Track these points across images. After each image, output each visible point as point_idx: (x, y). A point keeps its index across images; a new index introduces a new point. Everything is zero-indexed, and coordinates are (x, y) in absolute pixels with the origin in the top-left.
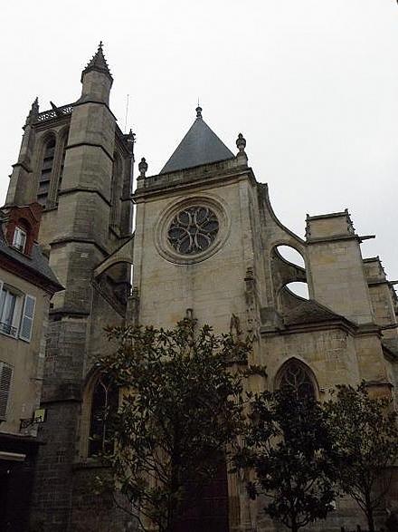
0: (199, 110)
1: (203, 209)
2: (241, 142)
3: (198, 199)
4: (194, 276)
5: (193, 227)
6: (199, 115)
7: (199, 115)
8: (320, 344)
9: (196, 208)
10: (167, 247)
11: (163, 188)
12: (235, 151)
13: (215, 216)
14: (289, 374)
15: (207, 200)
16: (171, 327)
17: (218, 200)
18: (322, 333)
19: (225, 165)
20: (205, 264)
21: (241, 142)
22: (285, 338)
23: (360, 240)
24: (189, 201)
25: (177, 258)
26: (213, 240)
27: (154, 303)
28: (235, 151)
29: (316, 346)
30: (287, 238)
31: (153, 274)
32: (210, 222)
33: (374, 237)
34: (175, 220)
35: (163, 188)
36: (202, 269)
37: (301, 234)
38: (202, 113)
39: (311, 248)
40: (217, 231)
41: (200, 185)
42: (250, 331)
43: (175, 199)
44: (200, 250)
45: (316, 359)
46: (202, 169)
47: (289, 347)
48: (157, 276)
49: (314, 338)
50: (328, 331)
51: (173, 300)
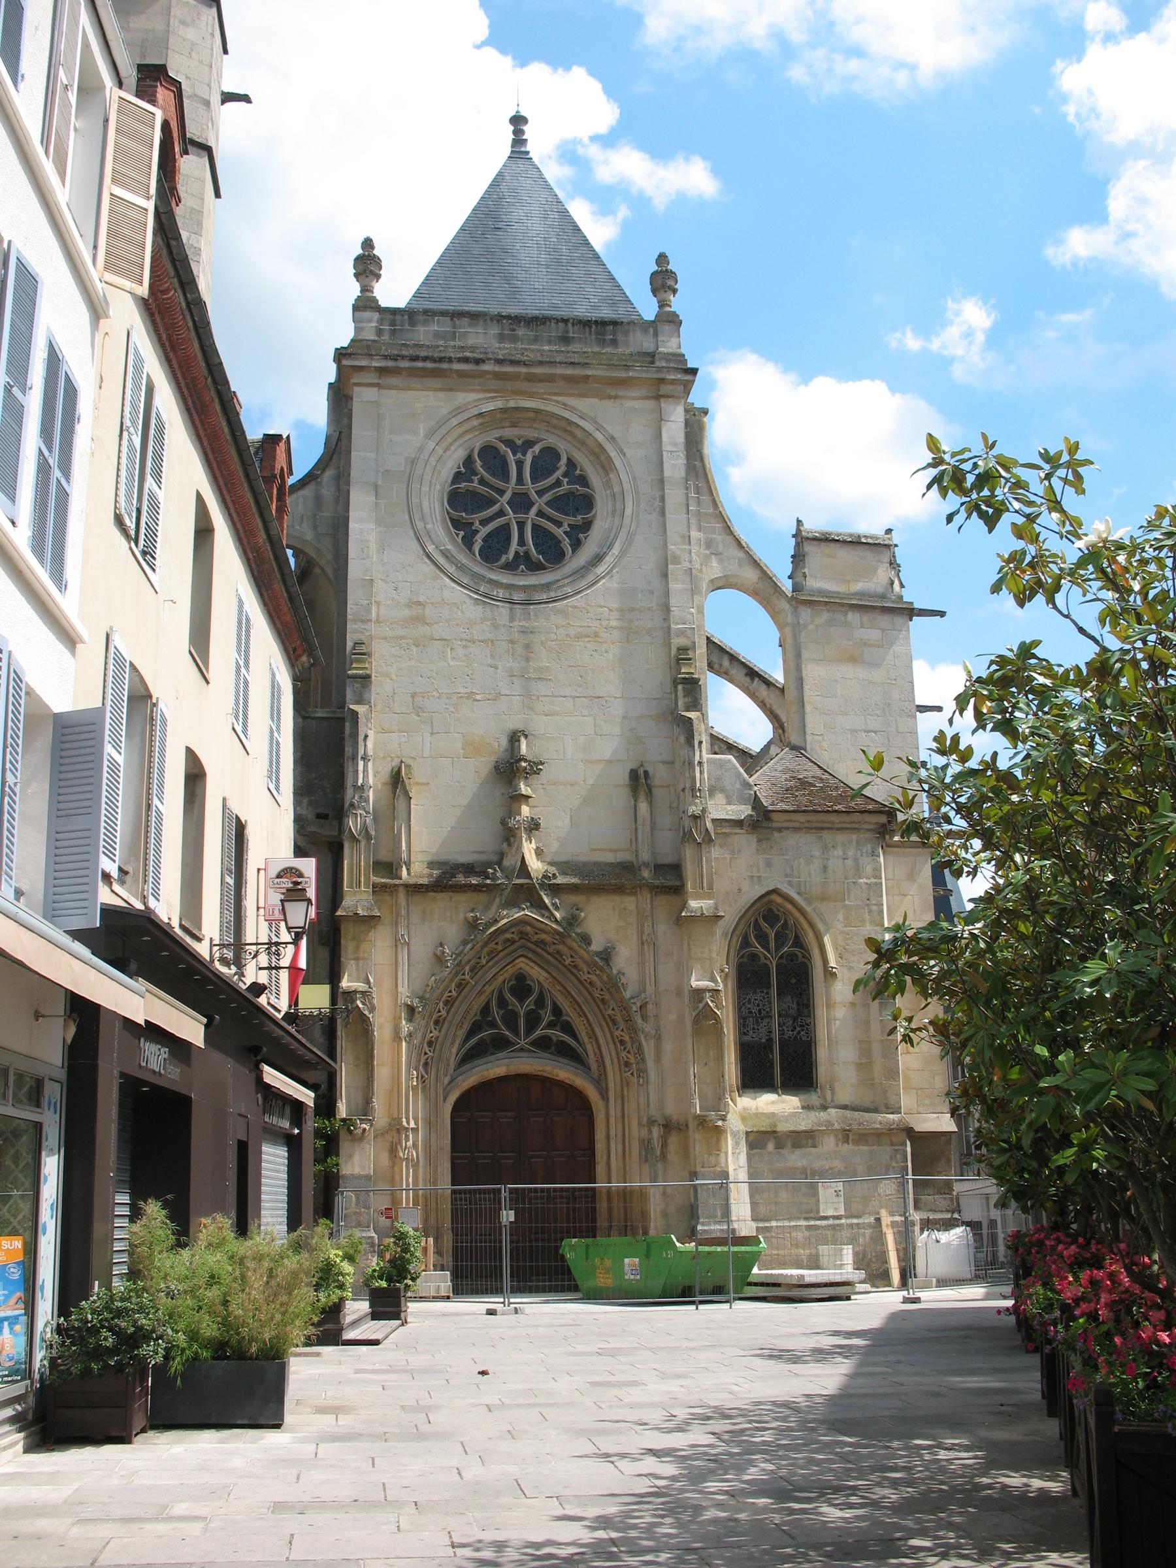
0: (518, 121)
1: (551, 453)
2: (663, 281)
6: (519, 140)
7: (519, 140)
8: (835, 864)
9: (529, 444)
11: (441, 360)
12: (648, 308)
13: (583, 481)
14: (502, 1002)
15: (567, 428)
16: (930, 917)
17: (599, 437)
18: (841, 837)
19: (620, 338)
20: (563, 613)
21: (663, 281)
22: (759, 841)
23: (911, 612)
24: (510, 416)
25: (475, 576)
26: (576, 545)
27: (413, 695)
28: (648, 308)
29: (825, 869)
30: (751, 575)
31: (406, 612)
32: (570, 495)
33: (942, 614)
34: (468, 462)
35: (441, 360)
36: (551, 622)
37: (781, 569)
38: (529, 131)
39: (805, 613)
40: (587, 526)
41: (550, 379)
43: (477, 400)
44: (535, 567)
45: (824, 898)
46: (554, 331)
47: (768, 864)
48: (420, 620)
49: (825, 849)
50: (854, 837)
51: (470, 695)
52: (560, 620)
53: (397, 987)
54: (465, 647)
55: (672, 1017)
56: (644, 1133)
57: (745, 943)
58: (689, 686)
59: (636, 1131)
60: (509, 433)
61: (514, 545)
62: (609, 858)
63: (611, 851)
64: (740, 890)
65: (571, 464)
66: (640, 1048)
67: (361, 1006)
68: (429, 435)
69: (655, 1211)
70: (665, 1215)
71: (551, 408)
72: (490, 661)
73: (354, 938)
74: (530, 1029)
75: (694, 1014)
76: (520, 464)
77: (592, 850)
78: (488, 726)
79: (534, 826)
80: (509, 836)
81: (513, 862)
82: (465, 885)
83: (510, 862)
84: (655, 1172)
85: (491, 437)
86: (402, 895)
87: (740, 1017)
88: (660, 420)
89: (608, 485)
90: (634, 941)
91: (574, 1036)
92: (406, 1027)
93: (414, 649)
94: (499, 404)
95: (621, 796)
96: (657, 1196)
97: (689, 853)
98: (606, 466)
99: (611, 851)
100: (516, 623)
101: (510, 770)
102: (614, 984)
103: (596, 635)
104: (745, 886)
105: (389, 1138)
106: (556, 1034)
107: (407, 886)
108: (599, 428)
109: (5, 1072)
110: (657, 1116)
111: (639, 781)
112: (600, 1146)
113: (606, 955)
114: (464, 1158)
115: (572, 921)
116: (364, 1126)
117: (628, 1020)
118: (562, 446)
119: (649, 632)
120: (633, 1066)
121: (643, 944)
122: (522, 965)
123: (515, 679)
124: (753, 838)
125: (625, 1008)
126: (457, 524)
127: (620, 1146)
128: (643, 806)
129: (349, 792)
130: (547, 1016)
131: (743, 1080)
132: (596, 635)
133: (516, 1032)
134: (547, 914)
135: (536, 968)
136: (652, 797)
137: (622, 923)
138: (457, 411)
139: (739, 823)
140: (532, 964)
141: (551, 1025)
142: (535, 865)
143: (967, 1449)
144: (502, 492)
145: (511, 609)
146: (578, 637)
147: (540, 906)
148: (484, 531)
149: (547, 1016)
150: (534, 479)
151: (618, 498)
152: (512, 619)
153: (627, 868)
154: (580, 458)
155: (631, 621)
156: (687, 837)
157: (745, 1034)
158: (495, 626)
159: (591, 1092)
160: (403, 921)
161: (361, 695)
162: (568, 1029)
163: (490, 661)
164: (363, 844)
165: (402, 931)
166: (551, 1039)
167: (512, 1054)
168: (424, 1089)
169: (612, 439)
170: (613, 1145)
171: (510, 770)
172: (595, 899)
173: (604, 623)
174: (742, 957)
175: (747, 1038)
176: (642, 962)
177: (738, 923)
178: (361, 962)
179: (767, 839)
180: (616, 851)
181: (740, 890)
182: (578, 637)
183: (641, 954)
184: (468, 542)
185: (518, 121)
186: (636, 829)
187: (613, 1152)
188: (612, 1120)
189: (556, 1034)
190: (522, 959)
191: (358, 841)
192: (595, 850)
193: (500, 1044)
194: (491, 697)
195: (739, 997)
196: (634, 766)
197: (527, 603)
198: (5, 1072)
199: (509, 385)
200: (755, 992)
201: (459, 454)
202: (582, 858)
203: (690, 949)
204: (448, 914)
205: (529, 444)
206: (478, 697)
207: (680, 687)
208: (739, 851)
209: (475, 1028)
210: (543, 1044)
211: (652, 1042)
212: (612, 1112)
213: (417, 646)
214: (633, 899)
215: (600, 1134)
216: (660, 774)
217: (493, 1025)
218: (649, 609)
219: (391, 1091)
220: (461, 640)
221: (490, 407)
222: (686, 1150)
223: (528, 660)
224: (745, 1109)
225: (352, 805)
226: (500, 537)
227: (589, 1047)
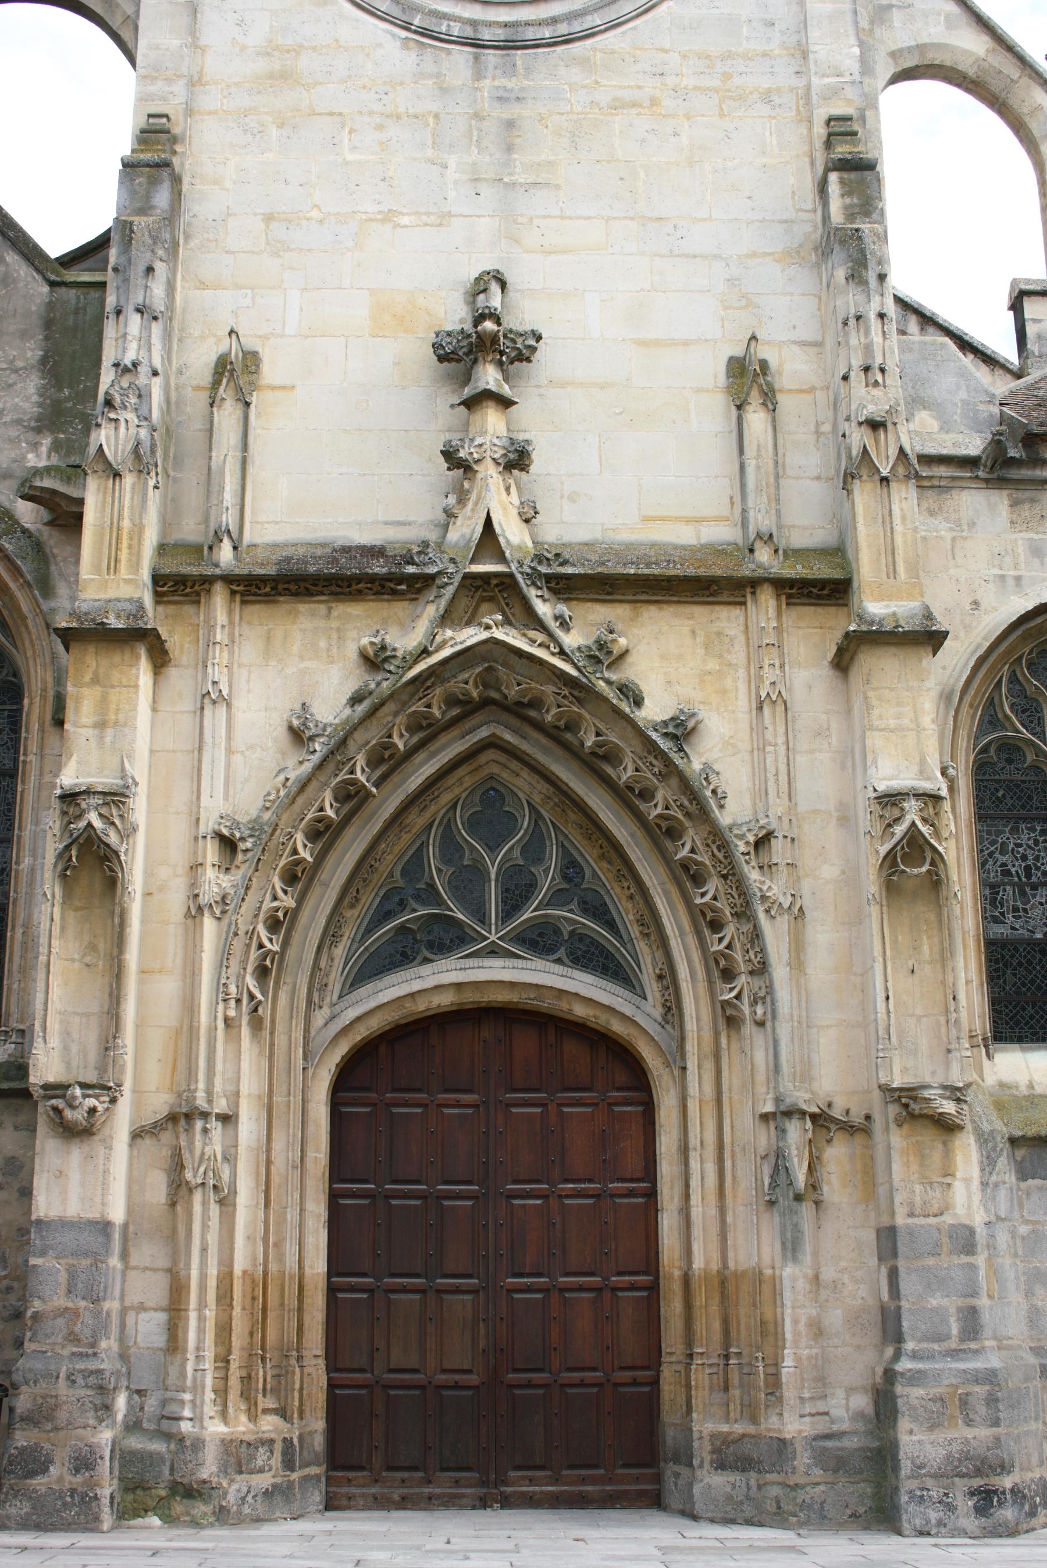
4: (513, 111)
14: (450, 847)
20: (584, 62)
22: (1015, 504)
42: (875, 425)
48: (284, 77)
51: (388, 217)
52: (576, 75)
53: (198, 798)
54: (380, 128)
55: (829, 871)
56: (763, 1139)
57: (991, 719)
58: (853, 175)
59: (749, 1135)
63: (689, 521)
64: (976, 603)
66: (756, 936)
67: (98, 824)
69: (795, 1322)
70: (818, 1330)
72: (430, 153)
73: (95, 681)
74: (511, 907)
75: (884, 850)
77: (646, 519)
81: (467, 531)
82: (359, 579)
84: (797, 1229)
86: (219, 597)
87: (985, 883)
90: (742, 703)
91: (611, 925)
92: (215, 882)
93: (274, 131)
95: (711, 411)
96: (801, 1284)
99: (689, 521)
100: (487, 83)
102: (697, 801)
103: (654, 102)
104: (988, 596)
105: (166, 1137)
106: (570, 916)
107: (229, 579)
110: (801, 1098)
112: (667, 1169)
113: (682, 730)
114: (528, 1289)
116: (92, 1102)
117: (732, 875)
119: (766, 97)
120: (738, 972)
121: (760, 708)
122: (495, 769)
123: (485, 189)
124: (1000, 500)
125: (718, 839)
127: (711, 1168)
129: (107, 377)
130: (548, 880)
131: (995, 1022)
132: (654, 102)
133: (483, 920)
134: (541, 637)
135: (525, 773)
136: (775, 404)
137: (713, 665)
139: (969, 462)
140: (515, 765)
141: (557, 898)
145: (476, 58)
146: (618, 105)
149: (548, 880)
152: (478, 76)
155: (727, 76)
157: (995, 920)
158: (444, 90)
160: (220, 656)
161: (148, 197)
162: (600, 912)
163: (430, 153)
164: (129, 480)
165: (217, 673)
166: (557, 931)
167: (470, 962)
168: (257, 1024)
170: (694, 1164)
171: (481, 353)
172: (650, 613)
173: (671, 81)
174: (985, 750)
175: (1000, 931)
176: (760, 747)
177: (975, 669)
178: (109, 733)
179: (1033, 501)
180: (699, 520)
181: (976, 603)
182: (618, 105)
183: (758, 729)
186: (742, 467)
187: (695, 1182)
188: (693, 1106)
189: (570, 916)
190: (491, 754)
191: (117, 475)
192: (654, 519)
193: (445, 938)
194: (432, 219)
195: (980, 840)
196: (739, 351)
197: (510, 45)
200: (1015, 830)
202: (624, 536)
203: (869, 707)
204: (323, 644)
206: (405, 220)
207: (833, 177)
208: (972, 524)
210: (539, 941)
211: (783, 922)
212: (693, 1088)
213: (281, 126)
214: (736, 612)
215: (666, 1143)
217: (430, 896)
218: (765, 55)
219: (178, 1032)
220: (371, 113)
222: (870, 1181)
223: (510, 148)
224: (1002, 1085)
225: (109, 403)
227: (642, 947)
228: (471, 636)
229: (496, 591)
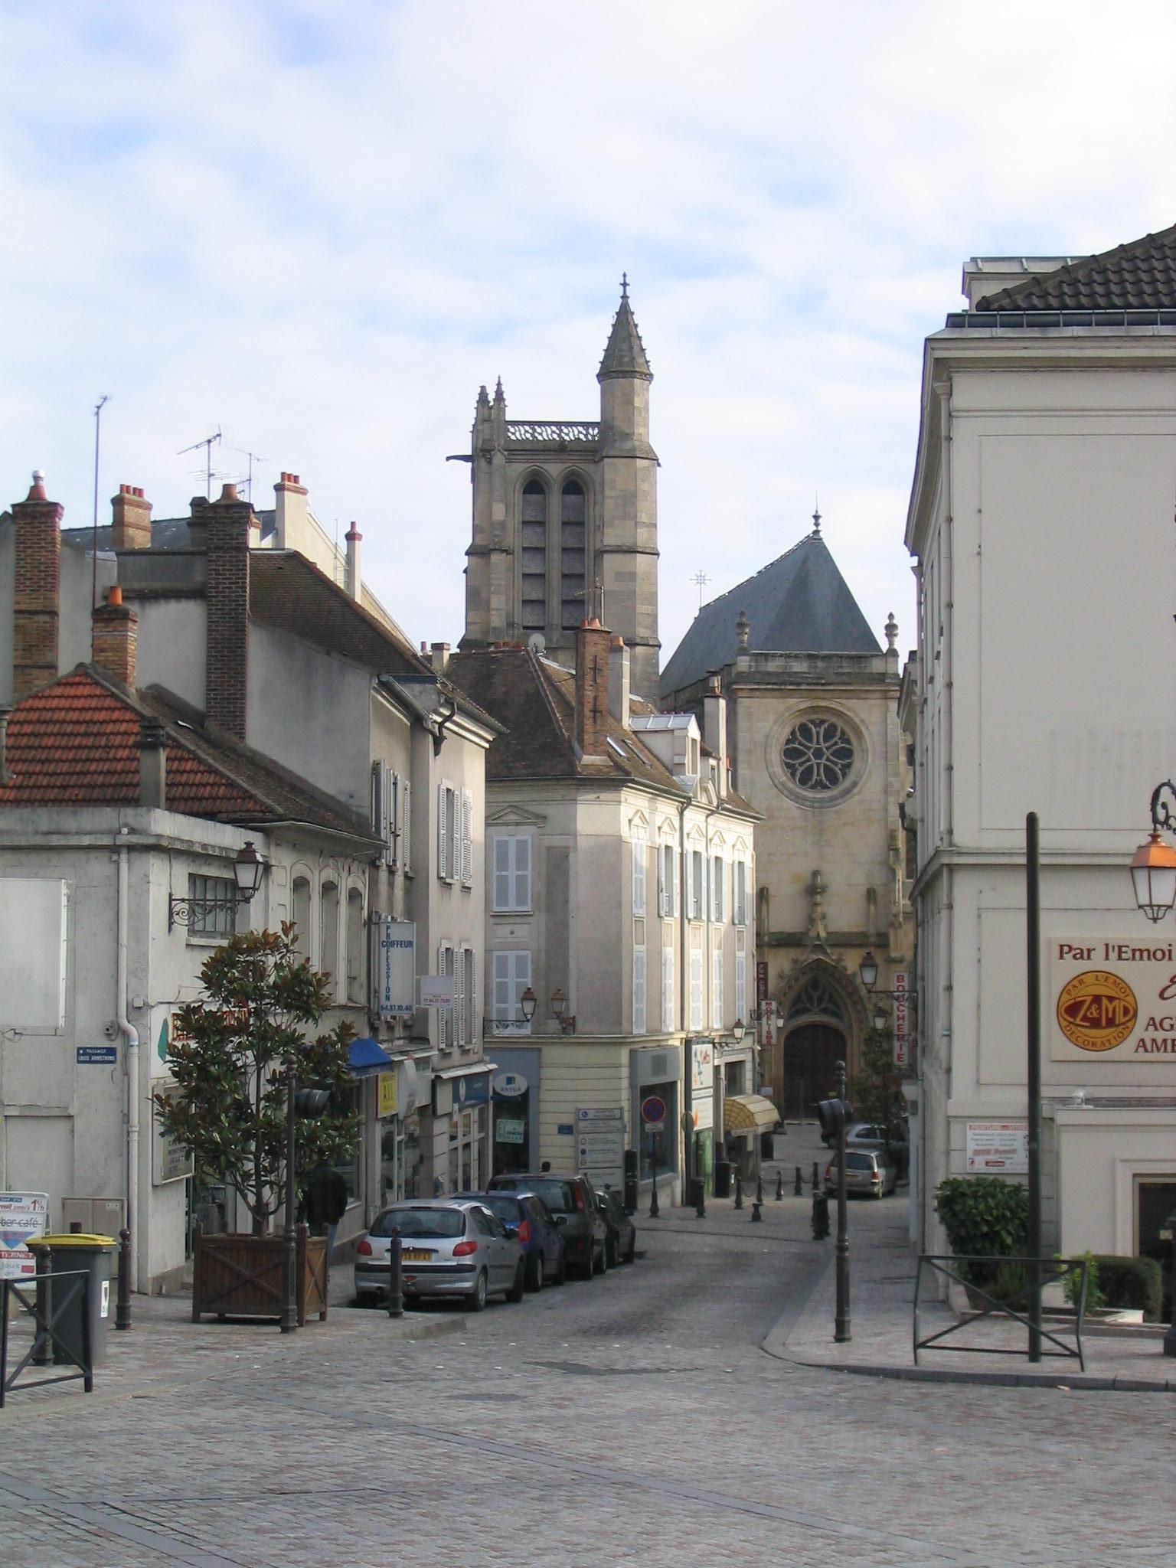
1: (833, 727)
3: (827, 709)
5: (818, 754)
9: (822, 722)
10: (779, 770)
13: (848, 741)
15: (840, 714)
17: (856, 720)
24: (814, 709)
26: (844, 775)
34: (793, 733)
40: (849, 765)
51: (794, 854)
60: (814, 717)
61: (815, 777)
62: (855, 930)
65: (843, 733)
68: (775, 722)
71: (834, 706)
76: (818, 733)
78: (803, 866)
79: (824, 917)
80: (811, 921)
83: (812, 934)
85: (804, 720)
86: (124, 851)
88: (887, 710)
89: (860, 744)
94: (808, 704)
97: (891, 933)
98: (859, 734)
101: (814, 889)
106: (831, 1006)
108: (857, 715)
109: (1173, 1051)
111: (871, 895)
115: (840, 960)
118: (839, 723)
126: (788, 765)
128: (872, 908)
138: (788, 709)
142: (823, 934)
143: (488, 741)
144: (809, 760)
146: (845, 824)
147: (825, 953)
148: (801, 769)
149: (826, 997)
150: (825, 741)
151: (865, 751)
153: (864, 934)
154: (848, 730)
156: (892, 925)
159: (846, 1033)
169: (863, 721)
171: (814, 889)
184: (793, 775)
185: (816, 517)
189: (831, 1006)
193: (805, 1010)
198: (1173, 1051)
199: (814, 694)
201: (788, 730)
205: (822, 722)
209: (794, 1003)
210: (824, 1011)
216: (880, 890)
221: (802, 706)
226: (808, 771)
228: (815, 957)
229: (820, 948)
